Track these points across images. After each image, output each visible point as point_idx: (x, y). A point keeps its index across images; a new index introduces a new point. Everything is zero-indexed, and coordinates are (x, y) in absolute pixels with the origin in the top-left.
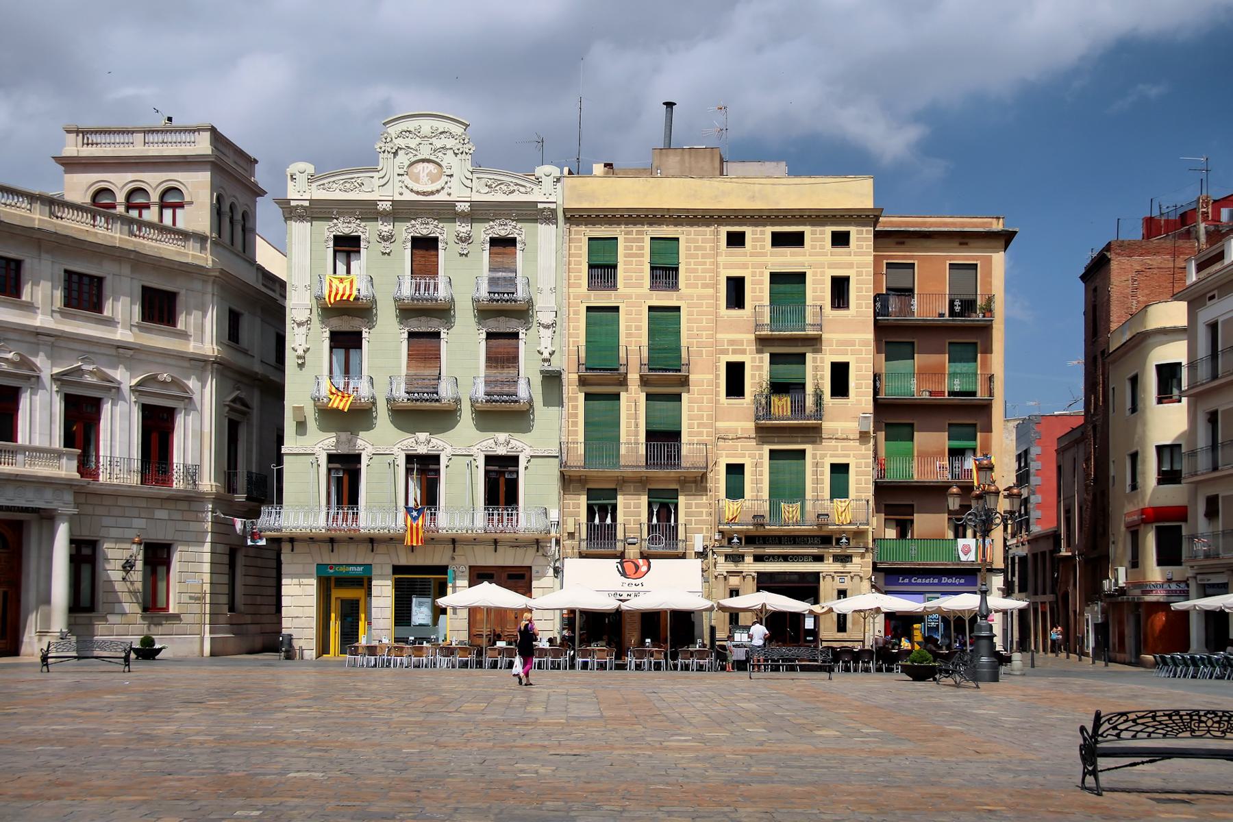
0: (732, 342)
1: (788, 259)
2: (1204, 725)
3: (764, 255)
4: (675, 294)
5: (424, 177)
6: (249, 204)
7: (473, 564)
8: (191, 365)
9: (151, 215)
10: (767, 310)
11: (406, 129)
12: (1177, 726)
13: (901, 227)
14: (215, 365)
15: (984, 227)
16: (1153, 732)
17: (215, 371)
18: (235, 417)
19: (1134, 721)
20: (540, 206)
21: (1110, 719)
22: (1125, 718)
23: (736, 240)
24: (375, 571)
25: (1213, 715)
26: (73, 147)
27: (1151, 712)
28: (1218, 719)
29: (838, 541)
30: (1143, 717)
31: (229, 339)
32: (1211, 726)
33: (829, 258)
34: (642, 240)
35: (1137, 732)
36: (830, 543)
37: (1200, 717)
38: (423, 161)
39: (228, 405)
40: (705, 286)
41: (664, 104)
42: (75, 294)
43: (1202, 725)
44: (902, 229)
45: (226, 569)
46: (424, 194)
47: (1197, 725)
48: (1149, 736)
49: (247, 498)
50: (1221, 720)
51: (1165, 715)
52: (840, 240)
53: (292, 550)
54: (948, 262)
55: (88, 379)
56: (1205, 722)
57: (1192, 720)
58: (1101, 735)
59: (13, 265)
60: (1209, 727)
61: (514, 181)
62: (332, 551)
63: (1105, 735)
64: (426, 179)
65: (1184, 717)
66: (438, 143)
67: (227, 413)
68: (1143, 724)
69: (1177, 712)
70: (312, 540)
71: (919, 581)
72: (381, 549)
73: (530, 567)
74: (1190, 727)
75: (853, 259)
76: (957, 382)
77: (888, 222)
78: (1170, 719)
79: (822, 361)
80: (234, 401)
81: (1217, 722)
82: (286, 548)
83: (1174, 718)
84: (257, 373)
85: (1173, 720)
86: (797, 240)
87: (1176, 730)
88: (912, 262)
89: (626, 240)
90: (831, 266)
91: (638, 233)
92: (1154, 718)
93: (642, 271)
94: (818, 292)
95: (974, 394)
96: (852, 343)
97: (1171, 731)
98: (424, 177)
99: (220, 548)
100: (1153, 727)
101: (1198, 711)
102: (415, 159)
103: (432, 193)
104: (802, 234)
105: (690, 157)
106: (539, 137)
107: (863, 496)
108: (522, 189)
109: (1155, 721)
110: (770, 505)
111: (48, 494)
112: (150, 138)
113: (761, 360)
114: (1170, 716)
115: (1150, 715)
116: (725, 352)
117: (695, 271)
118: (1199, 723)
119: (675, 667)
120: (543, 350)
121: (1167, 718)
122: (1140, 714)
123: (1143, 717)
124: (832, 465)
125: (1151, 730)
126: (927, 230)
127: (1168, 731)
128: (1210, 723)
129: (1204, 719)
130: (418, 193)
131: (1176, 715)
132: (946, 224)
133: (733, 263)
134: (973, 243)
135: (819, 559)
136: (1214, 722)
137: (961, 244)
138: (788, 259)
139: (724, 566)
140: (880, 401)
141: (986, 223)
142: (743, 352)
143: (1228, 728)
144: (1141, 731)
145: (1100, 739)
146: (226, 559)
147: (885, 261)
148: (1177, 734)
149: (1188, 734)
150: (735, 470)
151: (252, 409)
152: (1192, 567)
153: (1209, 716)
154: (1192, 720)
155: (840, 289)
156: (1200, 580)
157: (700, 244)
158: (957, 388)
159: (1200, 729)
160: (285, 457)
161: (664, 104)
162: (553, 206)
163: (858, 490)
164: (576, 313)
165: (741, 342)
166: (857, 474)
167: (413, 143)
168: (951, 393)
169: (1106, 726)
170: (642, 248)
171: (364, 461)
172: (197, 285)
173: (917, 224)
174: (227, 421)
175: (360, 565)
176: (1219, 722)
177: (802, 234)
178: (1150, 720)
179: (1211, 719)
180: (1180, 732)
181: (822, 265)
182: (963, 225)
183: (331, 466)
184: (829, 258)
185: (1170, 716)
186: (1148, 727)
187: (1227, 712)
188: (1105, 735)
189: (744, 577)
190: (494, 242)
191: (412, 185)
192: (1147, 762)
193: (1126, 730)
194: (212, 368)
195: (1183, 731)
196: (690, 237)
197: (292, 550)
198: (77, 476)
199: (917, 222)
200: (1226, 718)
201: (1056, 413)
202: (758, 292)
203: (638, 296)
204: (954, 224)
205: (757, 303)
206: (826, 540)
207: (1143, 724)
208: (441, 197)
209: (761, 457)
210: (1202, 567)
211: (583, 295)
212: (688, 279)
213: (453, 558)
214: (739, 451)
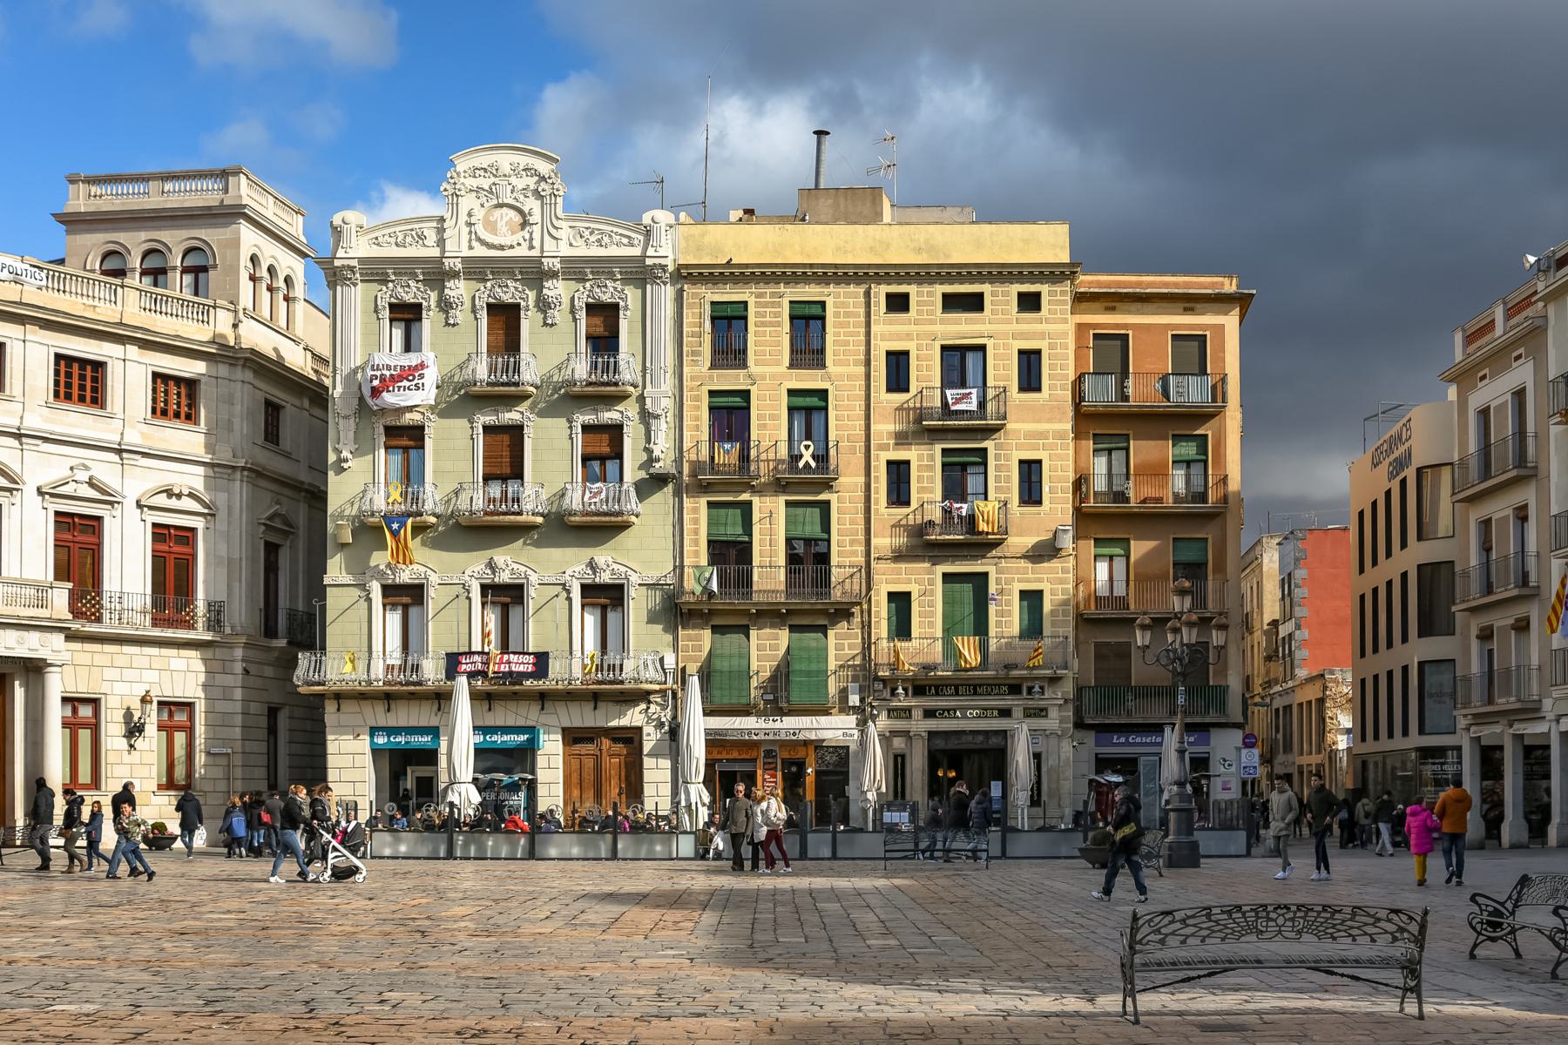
1: (963, 328)
2: (1273, 924)
3: (932, 322)
4: (820, 372)
6: (294, 267)
7: (567, 724)
8: (214, 472)
11: (480, 166)
12: (1239, 926)
13: (1110, 288)
14: (246, 473)
15: (1213, 289)
16: (1208, 936)
17: (245, 479)
18: (274, 539)
19: (1183, 921)
21: (1151, 920)
22: (1169, 918)
23: (898, 303)
25: (1285, 911)
26: (81, 200)
27: (1205, 909)
28: (1291, 915)
29: (1030, 690)
30: (1193, 917)
31: (266, 439)
32: (1283, 926)
33: (1015, 327)
35: (1187, 936)
36: (1020, 692)
37: (1268, 913)
39: (264, 524)
40: (856, 363)
41: (815, 133)
43: (1270, 924)
44: (1113, 290)
45: (263, 734)
46: (502, 248)
47: (1264, 924)
48: (1203, 941)
49: (289, 643)
50: (1295, 917)
51: (1223, 912)
52: (1030, 303)
53: (338, 710)
54: (1170, 333)
56: (1275, 920)
57: (1258, 918)
58: (1140, 942)
59: (946, 468)
60: (1280, 927)
61: (615, 230)
62: (389, 710)
63: (1144, 941)
64: (505, 229)
65: (1248, 914)
67: (263, 533)
68: (1194, 925)
69: (1239, 908)
70: (362, 696)
71: (1138, 740)
74: (1256, 927)
77: (1088, 281)
78: (1230, 918)
79: (1007, 458)
80: (270, 518)
81: (1289, 919)
82: (330, 707)
83: (1234, 916)
84: (303, 483)
85: (1233, 919)
86: (974, 303)
87: (1239, 932)
91: (773, 295)
92: (1209, 916)
93: (778, 344)
94: (1002, 370)
96: (1042, 435)
97: (1231, 934)
98: (502, 226)
99: (254, 708)
100: (1207, 928)
101: (1266, 906)
103: (512, 247)
104: (980, 296)
105: (846, 199)
107: (1061, 631)
108: (625, 241)
109: (1210, 921)
110: (943, 644)
111: (33, 638)
112: (168, 186)
113: (932, 458)
114: (1229, 913)
115: (1204, 912)
117: (847, 343)
118: (1267, 922)
119: (931, 849)
121: (1225, 916)
122: (1190, 913)
123: (1193, 917)
124: (1021, 592)
125: (1207, 932)
126: (1142, 291)
127: (1227, 934)
128: (1281, 921)
129: (1273, 915)
131: (1237, 912)
132: (1166, 285)
133: (890, 333)
135: (1005, 713)
136: (1286, 920)
138: (963, 328)
140: (1084, 510)
141: (1216, 283)
143: (1304, 927)
144: (1193, 935)
145: (1138, 947)
146: (263, 722)
147: (1091, 332)
148: (1240, 937)
149: (1253, 938)
150: (901, 601)
151: (298, 528)
152: (1465, 716)
153: (1279, 911)
154: (1258, 918)
155: (1030, 368)
156: (1475, 732)
157: (851, 309)
159: (1269, 929)
160: (328, 589)
161: (815, 133)
162: (662, 261)
169: (1145, 930)
173: (1130, 285)
174: (262, 542)
176: (1292, 920)
177: (980, 296)
178: (1204, 919)
179: (1283, 915)
180: (1243, 935)
181: (1005, 335)
182: (1187, 285)
183: (386, 601)
184: (1015, 327)
185: (1229, 913)
186: (1201, 929)
187: (1303, 906)
188: (1144, 941)
190: (1022, 297)
192: (1205, 976)
193: (1173, 933)
194: (242, 476)
195: (1247, 933)
196: (762, 300)
197: (338, 710)
198: (70, 616)
199: (1130, 282)
200: (1302, 914)
201: (1329, 527)
202: (926, 372)
203: (773, 376)
204: (1176, 285)
205: (924, 385)
206: (1015, 689)
207: (1194, 925)
208: (522, 251)
209: (931, 582)
210: (1475, 716)
211: (704, 377)
214: (904, 576)
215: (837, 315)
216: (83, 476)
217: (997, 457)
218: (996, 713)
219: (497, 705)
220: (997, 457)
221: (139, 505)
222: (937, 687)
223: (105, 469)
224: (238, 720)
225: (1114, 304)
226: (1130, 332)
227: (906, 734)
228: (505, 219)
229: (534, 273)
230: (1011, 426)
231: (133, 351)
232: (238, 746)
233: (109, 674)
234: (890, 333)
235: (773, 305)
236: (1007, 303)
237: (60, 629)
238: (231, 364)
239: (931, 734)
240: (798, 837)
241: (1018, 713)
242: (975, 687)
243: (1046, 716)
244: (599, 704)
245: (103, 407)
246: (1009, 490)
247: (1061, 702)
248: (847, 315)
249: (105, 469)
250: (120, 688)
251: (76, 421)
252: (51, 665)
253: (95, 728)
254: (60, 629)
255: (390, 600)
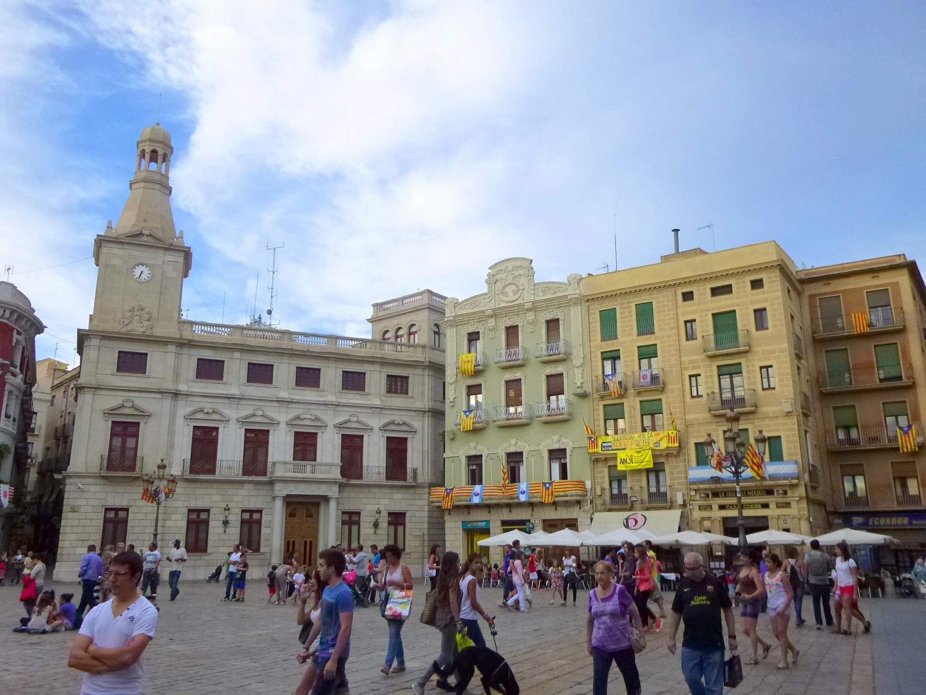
0: (691, 362)
1: (723, 303)
4: (652, 336)
5: (510, 294)
7: (502, 519)
9: (404, 340)
10: (712, 337)
20: (569, 297)
23: (688, 296)
24: (492, 525)
34: (630, 307)
38: (510, 284)
40: (671, 329)
41: (673, 231)
42: (393, 387)
46: (510, 302)
52: (757, 284)
55: (354, 425)
66: (516, 273)
72: (493, 511)
73: (576, 519)
75: (766, 296)
76: (881, 372)
86: (727, 289)
88: (837, 295)
89: (621, 308)
90: (752, 302)
94: (745, 321)
95: (900, 378)
96: (773, 352)
98: (510, 294)
102: (506, 284)
103: (514, 301)
104: (730, 286)
106: (605, 263)
116: (687, 369)
120: (576, 381)
130: (510, 302)
134: (881, 275)
135: (765, 506)
137: (873, 277)
138: (723, 303)
139: (697, 514)
142: (699, 367)
158: (882, 376)
161: (673, 231)
163: (789, 454)
164: (596, 357)
165: (697, 361)
166: (788, 442)
167: (503, 276)
168: (881, 380)
170: (630, 312)
171: (484, 459)
172: (419, 371)
175: (484, 521)
177: (730, 286)
189: (713, 521)
191: (506, 299)
198: (340, 477)
202: (704, 327)
206: (770, 492)
212: (660, 325)
213: (532, 515)
215: (658, 307)
216: (130, 404)
217: (748, 367)
218: (760, 506)
219: (514, 510)
220: (748, 367)
221: (287, 424)
222: (725, 493)
223: (273, 412)
224: (426, 520)
225: (828, 282)
226: (889, 288)
227: (709, 518)
228: (511, 290)
229: (520, 309)
230: (755, 349)
231: (377, 367)
232: (426, 532)
233: (364, 501)
234: (687, 310)
235: (627, 307)
236: (699, 295)
237: (336, 483)
238: (423, 369)
239: (725, 520)
240: (413, 576)
241: (772, 506)
242: (746, 491)
243: (790, 507)
244: (558, 508)
245: (407, 393)
246: (755, 383)
247: (798, 499)
248: (663, 306)
249: (273, 412)
250: (370, 507)
251: (353, 398)
252: (331, 498)
253: (358, 523)
254: (336, 483)
255: (470, 463)
